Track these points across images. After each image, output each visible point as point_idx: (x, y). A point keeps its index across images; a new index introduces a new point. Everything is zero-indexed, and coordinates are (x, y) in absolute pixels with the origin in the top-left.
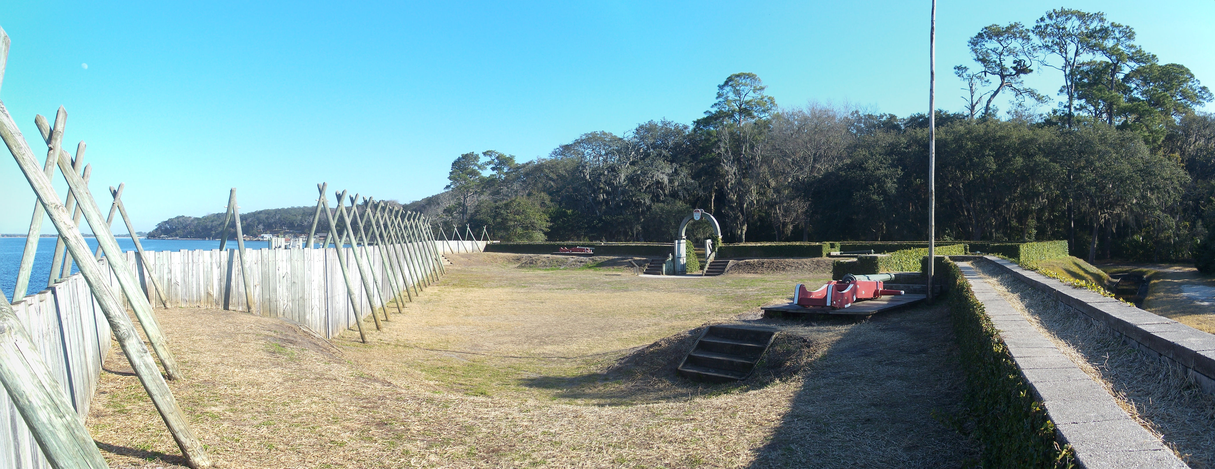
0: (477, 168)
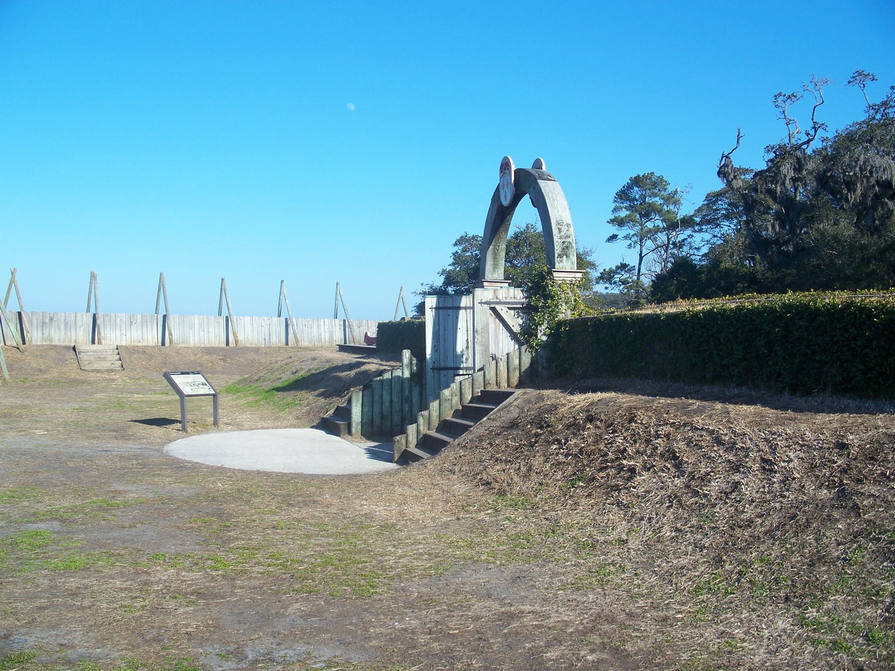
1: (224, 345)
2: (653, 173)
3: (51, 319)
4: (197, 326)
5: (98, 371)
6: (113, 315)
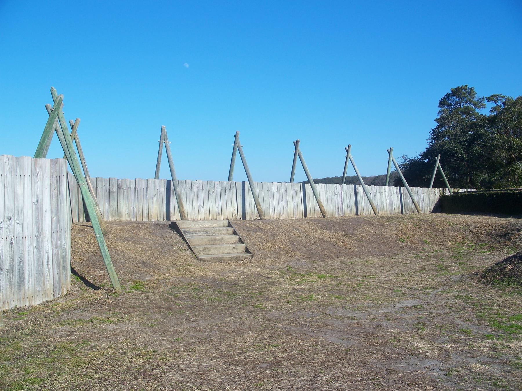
0: (472, 106)
1: (302, 216)
2: (466, 86)
3: (119, 187)
4: (276, 194)
5: (220, 261)
6: (188, 181)
